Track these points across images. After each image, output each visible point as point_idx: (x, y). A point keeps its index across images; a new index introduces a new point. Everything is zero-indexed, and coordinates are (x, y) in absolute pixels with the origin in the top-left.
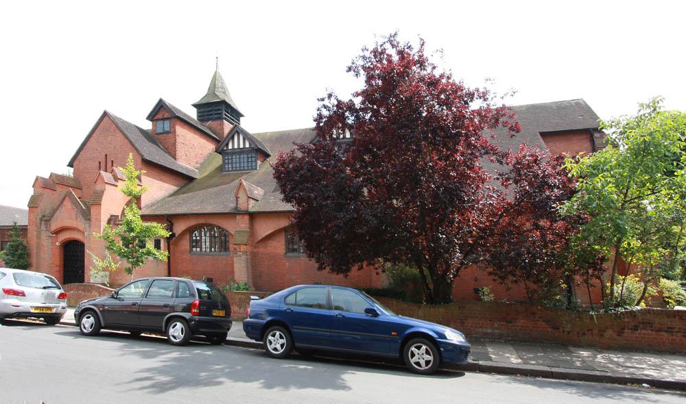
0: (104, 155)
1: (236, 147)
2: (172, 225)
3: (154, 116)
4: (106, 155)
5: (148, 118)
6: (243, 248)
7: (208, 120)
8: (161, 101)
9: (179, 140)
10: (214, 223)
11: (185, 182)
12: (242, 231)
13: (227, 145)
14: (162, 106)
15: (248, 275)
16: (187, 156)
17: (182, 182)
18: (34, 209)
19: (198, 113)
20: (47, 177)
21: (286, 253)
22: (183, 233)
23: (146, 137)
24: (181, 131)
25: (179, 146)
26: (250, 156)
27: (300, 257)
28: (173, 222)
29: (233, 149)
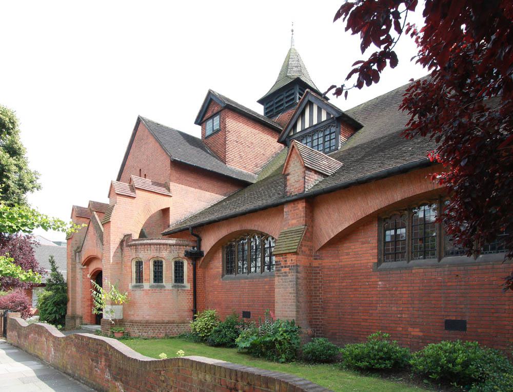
0: (138, 170)
1: (307, 126)
2: (200, 240)
3: (202, 119)
4: (140, 170)
5: (196, 123)
6: (291, 260)
7: (278, 113)
8: (210, 93)
9: (231, 137)
10: (253, 228)
11: (236, 189)
12: (291, 232)
13: (295, 127)
14: (211, 100)
15: (297, 307)
16: (241, 157)
17: (231, 190)
18: (70, 240)
19: (266, 109)
20: (86, 205)
21: (379, 262)
22: (214, 250)
23: (188, 141)
24: (234, 125)
25: (230, 146)
26: (327, 132)
27: (410, 268)
28: (201, 235)
29: (303, 130)
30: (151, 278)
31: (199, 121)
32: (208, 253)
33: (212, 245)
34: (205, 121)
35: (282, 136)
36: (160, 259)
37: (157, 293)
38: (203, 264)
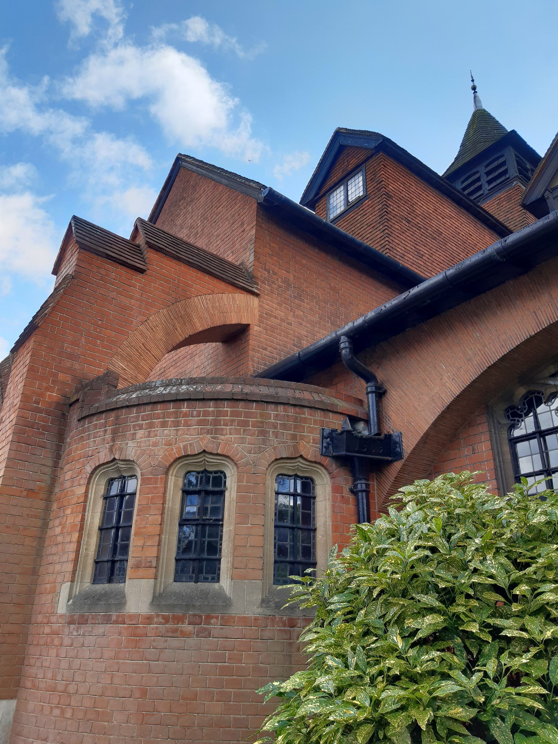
28: (380, 375)
30: (164, 555)
31: (311, 197)
32: (413, 453)
33: (448, 400)
34: (324, 195)
35: (532, 189)
36: (212, 466)
37: (184, 634)
38: (109, 623)
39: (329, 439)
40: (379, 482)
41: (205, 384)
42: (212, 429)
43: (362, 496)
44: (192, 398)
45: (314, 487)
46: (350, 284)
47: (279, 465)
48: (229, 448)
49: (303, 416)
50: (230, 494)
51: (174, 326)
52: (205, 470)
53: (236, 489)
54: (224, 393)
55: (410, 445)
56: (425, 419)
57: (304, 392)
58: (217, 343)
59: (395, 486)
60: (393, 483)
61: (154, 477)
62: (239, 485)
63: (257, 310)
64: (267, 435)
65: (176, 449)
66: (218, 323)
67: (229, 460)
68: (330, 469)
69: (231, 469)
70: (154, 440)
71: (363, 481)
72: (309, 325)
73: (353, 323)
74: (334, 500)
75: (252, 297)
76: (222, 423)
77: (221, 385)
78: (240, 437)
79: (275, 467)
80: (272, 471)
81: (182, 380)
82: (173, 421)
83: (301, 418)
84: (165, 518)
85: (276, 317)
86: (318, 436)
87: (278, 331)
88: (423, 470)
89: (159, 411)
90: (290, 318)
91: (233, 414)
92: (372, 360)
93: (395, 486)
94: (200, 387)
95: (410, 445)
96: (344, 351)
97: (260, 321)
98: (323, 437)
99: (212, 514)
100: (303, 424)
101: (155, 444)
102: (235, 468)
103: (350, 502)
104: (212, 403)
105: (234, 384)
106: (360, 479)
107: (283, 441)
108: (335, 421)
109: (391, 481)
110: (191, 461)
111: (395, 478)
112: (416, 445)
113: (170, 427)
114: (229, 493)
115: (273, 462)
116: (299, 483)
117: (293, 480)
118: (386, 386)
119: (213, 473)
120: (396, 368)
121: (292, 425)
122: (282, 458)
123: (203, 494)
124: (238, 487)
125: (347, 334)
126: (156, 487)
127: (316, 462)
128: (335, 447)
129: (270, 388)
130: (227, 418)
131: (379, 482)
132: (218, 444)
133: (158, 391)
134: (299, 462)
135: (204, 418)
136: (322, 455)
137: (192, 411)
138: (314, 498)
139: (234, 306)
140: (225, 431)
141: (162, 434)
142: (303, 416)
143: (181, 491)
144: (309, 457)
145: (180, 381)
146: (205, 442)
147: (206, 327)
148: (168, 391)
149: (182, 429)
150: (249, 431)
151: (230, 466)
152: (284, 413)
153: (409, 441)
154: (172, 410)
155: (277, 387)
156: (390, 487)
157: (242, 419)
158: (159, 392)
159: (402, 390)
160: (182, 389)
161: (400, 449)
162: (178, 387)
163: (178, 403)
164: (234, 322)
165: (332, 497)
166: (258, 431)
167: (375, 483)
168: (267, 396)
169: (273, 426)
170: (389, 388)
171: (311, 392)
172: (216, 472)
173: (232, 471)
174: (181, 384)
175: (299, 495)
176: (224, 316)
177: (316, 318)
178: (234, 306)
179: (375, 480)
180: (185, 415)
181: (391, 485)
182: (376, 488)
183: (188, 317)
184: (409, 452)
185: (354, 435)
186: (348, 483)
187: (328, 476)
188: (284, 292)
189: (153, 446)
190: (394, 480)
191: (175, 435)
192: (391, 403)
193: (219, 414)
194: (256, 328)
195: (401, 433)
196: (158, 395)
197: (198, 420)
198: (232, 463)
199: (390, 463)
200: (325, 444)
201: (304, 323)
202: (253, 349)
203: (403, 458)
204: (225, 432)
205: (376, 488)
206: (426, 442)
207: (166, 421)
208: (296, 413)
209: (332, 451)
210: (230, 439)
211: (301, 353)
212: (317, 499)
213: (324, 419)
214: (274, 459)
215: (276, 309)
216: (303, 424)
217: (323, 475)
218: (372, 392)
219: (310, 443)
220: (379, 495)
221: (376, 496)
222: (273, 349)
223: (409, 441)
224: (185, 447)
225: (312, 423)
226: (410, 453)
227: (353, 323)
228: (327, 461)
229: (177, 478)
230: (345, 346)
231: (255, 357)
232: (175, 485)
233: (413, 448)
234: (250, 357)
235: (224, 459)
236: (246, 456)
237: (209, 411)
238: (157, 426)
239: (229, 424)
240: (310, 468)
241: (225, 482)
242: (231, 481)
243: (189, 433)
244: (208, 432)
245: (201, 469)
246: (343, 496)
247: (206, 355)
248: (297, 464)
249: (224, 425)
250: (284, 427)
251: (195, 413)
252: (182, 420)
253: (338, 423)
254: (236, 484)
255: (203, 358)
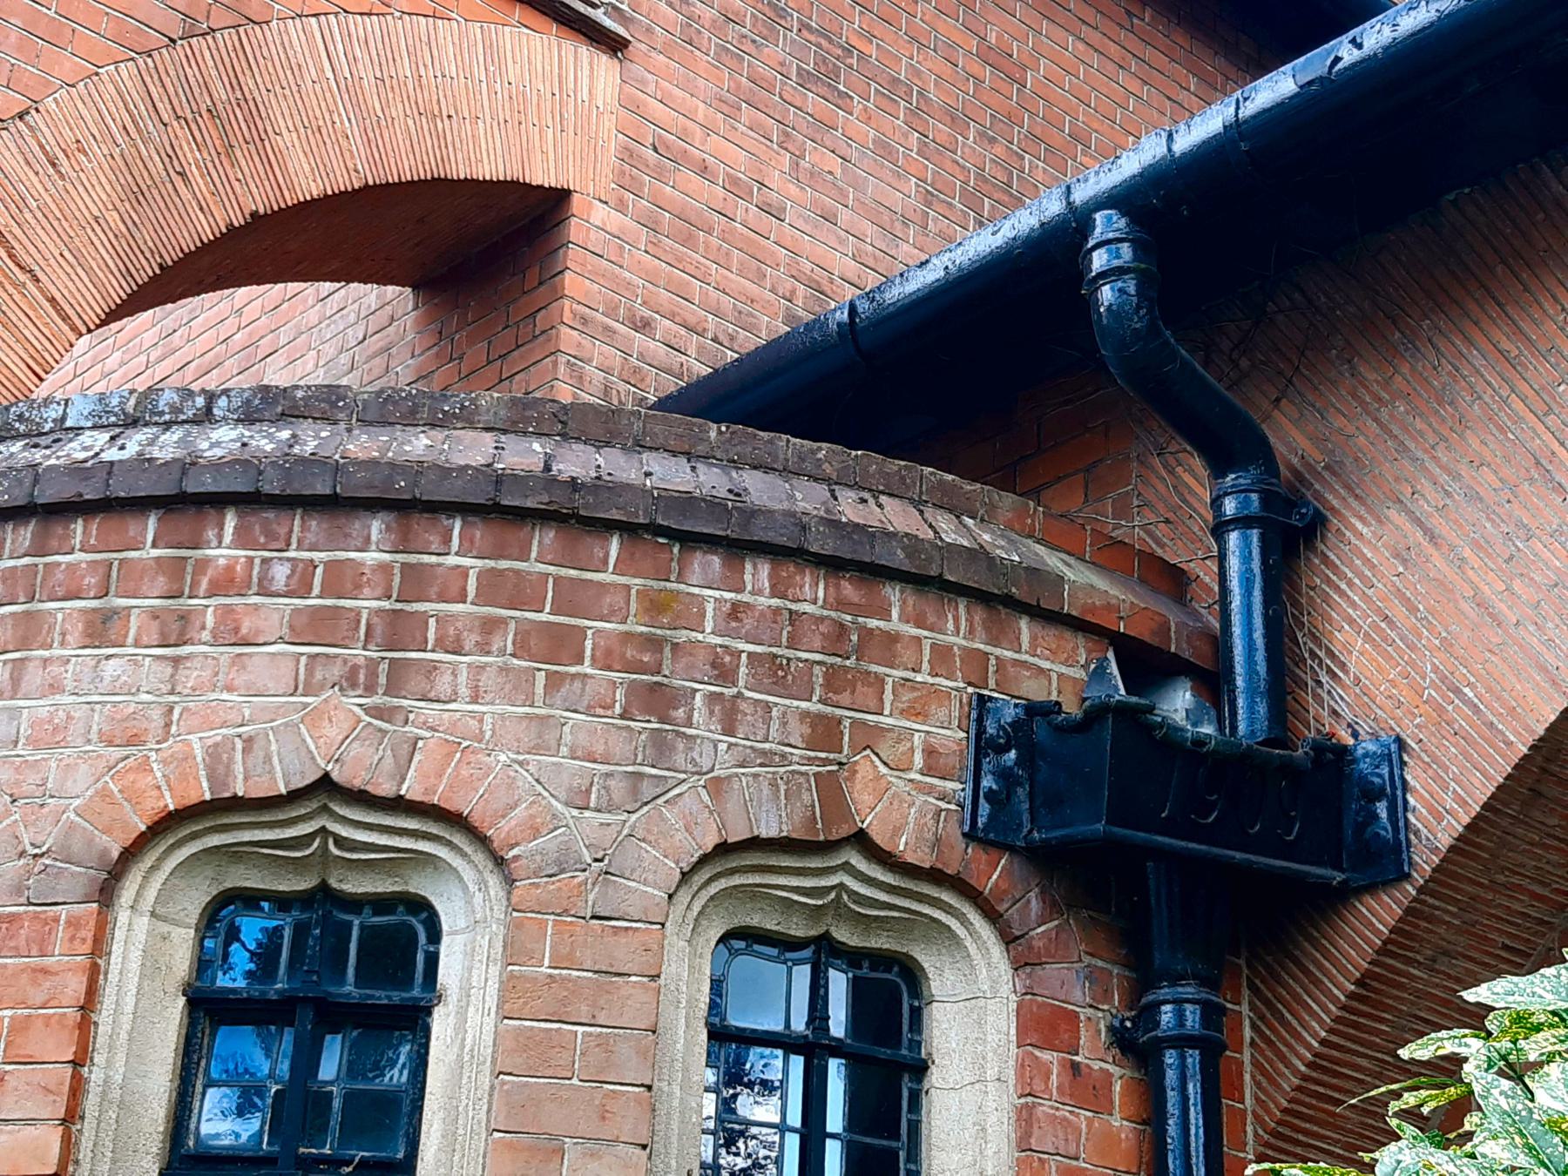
39: (1013, 754)
40: (1267, 1003)
41: (342, 426)
42: (372, 665)
43: (1183, 1067)
44: (267, 489)
45: (917, 1015)
46: (1081, 46)
47: (737, 880)
48: (464, 772)
49: (873, 623)
50: (461, 1028)
51: (171, 156)
52: (324, 886)
53: (492, 1002)
54: (444, 472)
55: (1450, 803)
56: (1543, 669)
57: (883, 499)
58: (391, 290)
59: (1356, 1025)
60: (1344, 1008)
61: (36, 916)
62: (512, 976)
63: (609, 123)
64: (680, 713)
65: (164, 762)
66: (406, 166)
67: (458, 839)
68: (1013, 914)
69: (472, 887)
70: (43, 713)
71: (1188, 990)
72: (869, 229)
73: (1170, 137)
74: (1029, 1083)
75: (585, 51)
76: (431, 635)
77: (433, 433)
78: (527, 716)
79: (713, 889)
80: (696, 908)
81: (211, 397)
82: (155, 615)
83: (867, 633)
84: (86, 1143)
85: (703, 170)
86: (952, 737)
87: (714, 241)
88: (1506, 947)
89: (78, 556)
90: (775, 179)
91: (492, 591)
92: (1244, 363)
93: (1356, 1025)
94: (317, 437)
95: (1450, 803)
96: (1107, 294)
97: (628, 185)
98: (983, 746)
99: (353, 1129)
100: (874, 668)
101: (50, 736)
102: (494, 882)
103: (1112, 1102)
104: (376, 527)
105: (505, 432)
106: (1175, 980)
107: (764, 753)
108: (1046, 665)
109: (1334, 1000)
110: (247, 836)
111: (1358, 983)
112: (1485, 807)
113: (137, 644)
114: (452, 1020)
115: (704, 860)
116: (838, 984)
117: (807, 969)
118: (1318, 496)
119: (367, 910)
120: (1379, 400)
121: (817, 670)
122: (755, 844)
123: (306, 1017)
124: (509, 987)
125: (1120, 199)
126: (45, 971)
127: (935, 876)
128: (1047, 803)
129: (701, 467)
130: (460, 607)
131: (1267, 1003)
132: (406, 747)
133: (75, 450)
134: (847, 867)
135: (329, 602)
136: (970, 836)
137: (265, 561)
138: (920, 1069)
139: (492, 92)
140: (447, 678)
141: (87, 679)
142: (873, 623)
143: (182, 1001)
144: (904, 846)
145: (200, 401)
146: (333, 732)
147: (343, 181)
148: (132, 449)
149: (206, 656)
150: (577, 684)
151: (468, 874)
152: (775, 602)
153: (1445, 788)
154: (156, 553)
155: (735, 464)
156: (1331, 1031)
157: (543, 617)
158: (82, 455)
159: (1410, 513)
160: (212, 446)
161: (1396, 829)
162: (189, 434)
163: (184, 523)
164: (487, 170)
165: (1021, 1067)
166: (632, 688)
167: (1245, 1009)
168: (686, 502)
169: (714, 665)
170: (1335, 503)
171: (918, 504)
172: (382, 903)
173: (478, 898)
174: (206, 417)
175: (836, 1049)
176: (441, 137)
177: (904, 196)
178: (492, 92)
179: (1246, 993)
180: (226, 584)
181: (1337, 1020)
182: (1248, 1033)
183: (250, 120)
184: (1444, 841)
185: (1159, 734)
186: (1106, 996)
187: (997, 951)
188: (748, 47)
189: (35, 743)
190: (1351, 996)
191: (165, 688)
192: (1350, 584)
193: (416, 582)
194: (600, 214)
195: (1401, 744)
196: (77, 470)
197: (296, 611)
198: (479, 857)
199: (1337, 899)
200: (987, 782)
201: (844, 216)
202: (585, 320)
203: (1408, 876)
204: (443, 685)
205: (1248, 1033)
206: (1540, 794)
207: (115, 611)
208: (841, 605)
209: (1026, 817)
210: (473, 723)
211: (863, 306)
212: (935, 1077)
213: (988, 649)
214: (710, 842)
215: (708, 129)
216: (874, 668)
217: (972, 949)
218: (1242, 522)
219: (909, 769)
220: (1264, 1073)
221: (1247, 1077)
222: (683, 332)
223: (1445, 788)
224: (216, 757)
225: (925, 666)
226: (1452, 849)
227: (1170, 137)
228: (995, 874)
229: (164, 928)
230: (1116, 263)
231: (588, 361)
232: (152, 965)
233: (1466, 820)
234: (563, 359)
235: (434, 829)
236: (556, 822)
237: (362, 564)
238: (63, 634)
239: (470, 641)
240: (906, 903)
241: (432, 961)
242: (470, 953)
243: (240, 680)
244: (349, 681)
245: (303, 883)
246: (1075, 1067)
247: (329, 350)
248: (833, 880)
249: (441, 645)
250: (774, 673)
251: (280, 573)
252: (208, 609)
253: (1060, 676)
254: (494, 970)
255: (310, 366)
